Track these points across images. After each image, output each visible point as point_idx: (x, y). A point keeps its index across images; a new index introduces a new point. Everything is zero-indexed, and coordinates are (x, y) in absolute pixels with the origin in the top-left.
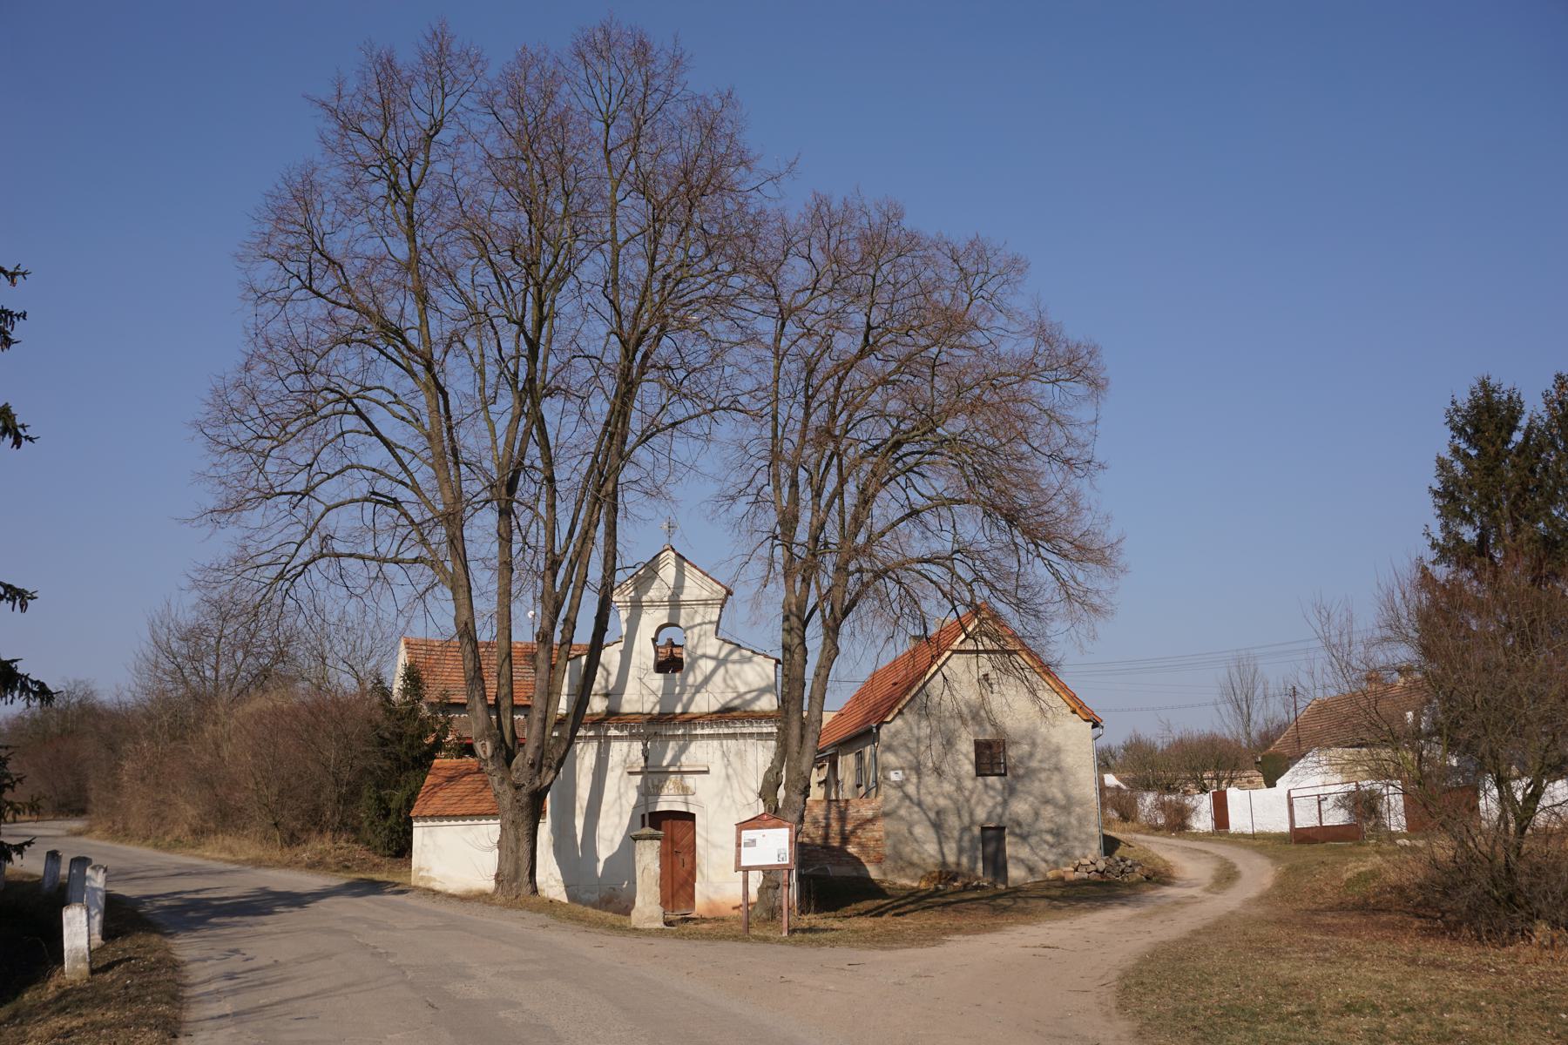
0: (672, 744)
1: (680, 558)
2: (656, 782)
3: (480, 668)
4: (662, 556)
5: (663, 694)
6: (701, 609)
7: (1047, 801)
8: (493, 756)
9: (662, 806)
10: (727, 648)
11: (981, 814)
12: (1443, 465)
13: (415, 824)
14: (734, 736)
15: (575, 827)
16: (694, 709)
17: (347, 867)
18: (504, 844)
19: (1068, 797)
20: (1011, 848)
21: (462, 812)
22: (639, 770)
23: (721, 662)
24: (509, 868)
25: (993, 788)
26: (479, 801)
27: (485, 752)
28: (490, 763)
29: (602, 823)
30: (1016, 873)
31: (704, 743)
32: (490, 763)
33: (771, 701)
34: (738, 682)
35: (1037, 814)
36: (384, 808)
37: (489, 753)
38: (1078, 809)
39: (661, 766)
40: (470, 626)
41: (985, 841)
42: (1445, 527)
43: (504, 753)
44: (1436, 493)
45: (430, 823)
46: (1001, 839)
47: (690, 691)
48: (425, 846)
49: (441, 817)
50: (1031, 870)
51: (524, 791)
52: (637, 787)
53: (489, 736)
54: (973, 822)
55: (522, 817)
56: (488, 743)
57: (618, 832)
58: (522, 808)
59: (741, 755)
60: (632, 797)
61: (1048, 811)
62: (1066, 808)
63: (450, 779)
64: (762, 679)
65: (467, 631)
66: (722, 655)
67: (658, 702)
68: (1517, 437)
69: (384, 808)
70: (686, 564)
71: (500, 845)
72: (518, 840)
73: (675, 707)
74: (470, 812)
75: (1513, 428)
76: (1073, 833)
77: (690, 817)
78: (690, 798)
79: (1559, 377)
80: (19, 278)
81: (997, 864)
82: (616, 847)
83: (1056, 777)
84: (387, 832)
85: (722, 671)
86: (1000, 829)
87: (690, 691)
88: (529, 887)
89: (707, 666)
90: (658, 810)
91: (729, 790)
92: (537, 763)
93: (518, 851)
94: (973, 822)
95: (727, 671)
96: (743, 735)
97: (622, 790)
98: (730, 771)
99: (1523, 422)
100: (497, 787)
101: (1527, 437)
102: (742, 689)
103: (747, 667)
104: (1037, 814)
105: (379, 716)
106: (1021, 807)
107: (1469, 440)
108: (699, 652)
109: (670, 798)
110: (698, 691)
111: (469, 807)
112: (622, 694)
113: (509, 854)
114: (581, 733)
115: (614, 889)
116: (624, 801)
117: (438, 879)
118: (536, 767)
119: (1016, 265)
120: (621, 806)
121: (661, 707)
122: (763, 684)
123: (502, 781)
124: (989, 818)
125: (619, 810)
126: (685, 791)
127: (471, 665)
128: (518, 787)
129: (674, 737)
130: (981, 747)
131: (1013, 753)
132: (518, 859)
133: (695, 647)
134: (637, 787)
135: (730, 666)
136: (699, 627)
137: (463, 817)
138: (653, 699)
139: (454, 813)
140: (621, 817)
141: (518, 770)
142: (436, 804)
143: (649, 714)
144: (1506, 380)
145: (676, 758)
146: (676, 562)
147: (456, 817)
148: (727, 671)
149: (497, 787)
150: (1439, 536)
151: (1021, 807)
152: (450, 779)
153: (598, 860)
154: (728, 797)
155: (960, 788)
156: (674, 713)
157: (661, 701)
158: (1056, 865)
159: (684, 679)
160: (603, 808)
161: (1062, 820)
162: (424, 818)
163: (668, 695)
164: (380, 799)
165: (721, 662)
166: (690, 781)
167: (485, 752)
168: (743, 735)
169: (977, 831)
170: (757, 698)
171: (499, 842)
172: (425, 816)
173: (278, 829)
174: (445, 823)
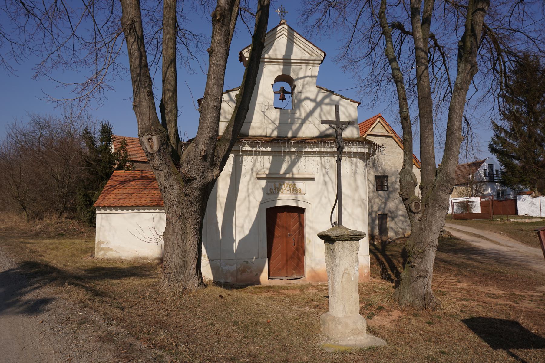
0: (287, 158)
2: (277, 186)
3: (146, 66)
4: (279, 28)
5: (279, 124)
6: (304, 66)
8: (159, 150)
9: (279, 203)
13: (97, 212)
15: (217, 217)
17: (63, 235)
18: (171, 237)
20: (390, 224)
21: (131, 204)
22: (265, 176)
25: (380, 196)
26: (141, 197)
27: (151, 147)
28: (157, 157)
31: (311, 158)
32: (157, 157)
33: (352, 131)
36: (88, 201)
37: (156, 147)
39: (279, 174)
40: (137, 25)
43: (170, 150)
45: (108, 211)
48: (103, 226)
49: (116, 207)
51: (195, 184)
52: (263, 188)
53: (155, 131)
55: (191, 212)
56: (155, 138)
57: (247, 221)
58: (191, 202)
60: (258, 196)
63: (122, 183)
64: (347, 117)
66: (319, 99)
67: (275, 129)
69: (88, 201)
70: (295, 34)
72: (185, 233)
73: (288, 132)
74: (137, 204)
77: (301, 211)
78: (300, 198)
82: (247, 232)
84: (90, 214)
85: (318, 110)
88: (196, 279)
89: (308, 105)
90: (277, 205)
91: (326, 193)
92: (210, 156)
93: (185, 244)
95: (322, 110)
97: (250, 191)
98: (327, 179)
100: (164, 182)
105: (87, 151)
108: (303, 96)
109: (286, 197)
110: (304, 121)
111: (133, 200)
112: (251, 122)
113: (176, 246)
115: (247, 262)
116: (251, 198)
117: (114, 249)
118: (209, 160)
120: (249, 202)
121: (278, 132)
123: (169, 176)
125: (247, 205)
126: (296, 192)
127: (137, 63)
128: (188, 181)
129: (291, 153)
132: (185, 251)
134: (263, 188)
135: (324, 107)
136: (302, 80)
138: (271, 126)
139: (126, 205)
140: (249, 209)
141: (189, 162)
142: (111, 198)
143: (269, 137)
145: (290, 169)
146: (289, 33)
148: (322, 110)
149: (164, 182)
152: (122, 183)
153: (234, 241)
154: (325, 197)
156: (287, 137)
157: (278, 128)
160: (238, 203)
162: (104, 208)
164: (86, 196)
166: (300, 185)
167: (151, 147)
171: (164, 234)
172: (105, 206)
173: (26, 211)
174: (120, 211)
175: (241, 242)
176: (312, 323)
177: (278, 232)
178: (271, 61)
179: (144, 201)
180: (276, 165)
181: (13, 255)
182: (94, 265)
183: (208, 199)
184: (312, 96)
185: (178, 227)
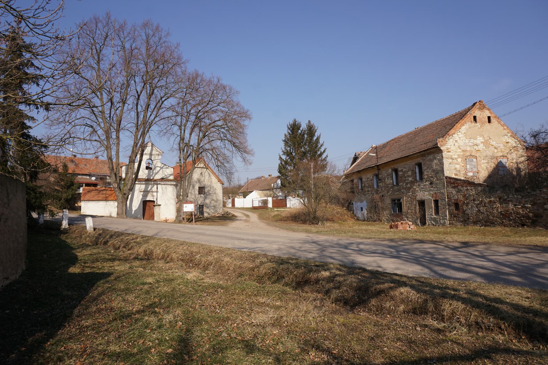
0: (150, 186)
1: (152, 145)
7: (213, 200)
9: (147, 199)
10: (163, 165)
11: (199, 203)
12: (285, 135)
14: (165, 184)
16: (155, 178)
19: (217, 200)
23: (161, 168)
24: (120, 212)
29: (133, 202)
30: (206, 215)
34: (165, 173)
35: (211, 203)
37: (116, 186)
38: (538, 192)
41: (200, 208)
42: (285, 148)
44: (283, 141)
46: (203, 208)
47: (154, 174)
49: (89, 201)
50: (209, 214)
54: (198, 204)
59: (166, 188)
60: (141, 197)
61: (213, 202)
62: (216, 201)
63: (89, 192)
65: (110, 159)
68: (300, 131)
71: (117, 207)
72: (123, 206)
75: (299, 129)
76: (217, 206)
79: (309, 121)
80: (42, 70)
81: (202, 213)
83: (215, 195)
85: (162, 170)
86: (203, 205)
87: (154, 174)
89: (158, 169)
94: (198, 204)
96: (167, 184)
99: (301, 129)
101: (301, 132)
102: (166, 174)
103: (167, 169)
104: (211, 203)
106: (207, 201)
107: (291, 131)
111: (96, 198)
114: (137, 182)
119: (237, 92)
122: (171, 173)
124: (201, 203)
126: (153, 196)
129: (151, 184)
130: (200, 188)
131: (206, 190)
133: (156, 164)
137: (95, 201)
144: (299, 120)
145: (151, 189)
147: (93, 201)
150: (284, 149)
151: (207, 201)
155: (195, 197)
158: (214, 213)
159: (153, 171)
160: (134, 199)
161: (216, 204)
163: (149, 174)
165: (161, 168)
168: (167, 184)
169: (198, 206)
170: (169, 176)
175: (135, 211)
176: (496, 344)
177: (147, 208)
178: (146, 154)
179: (100, 198)
180: (146, 188)
181: (290, 132)
182: (293, 251)
183: (430, 125)
184: (160, 166)
185: (121, 204)
